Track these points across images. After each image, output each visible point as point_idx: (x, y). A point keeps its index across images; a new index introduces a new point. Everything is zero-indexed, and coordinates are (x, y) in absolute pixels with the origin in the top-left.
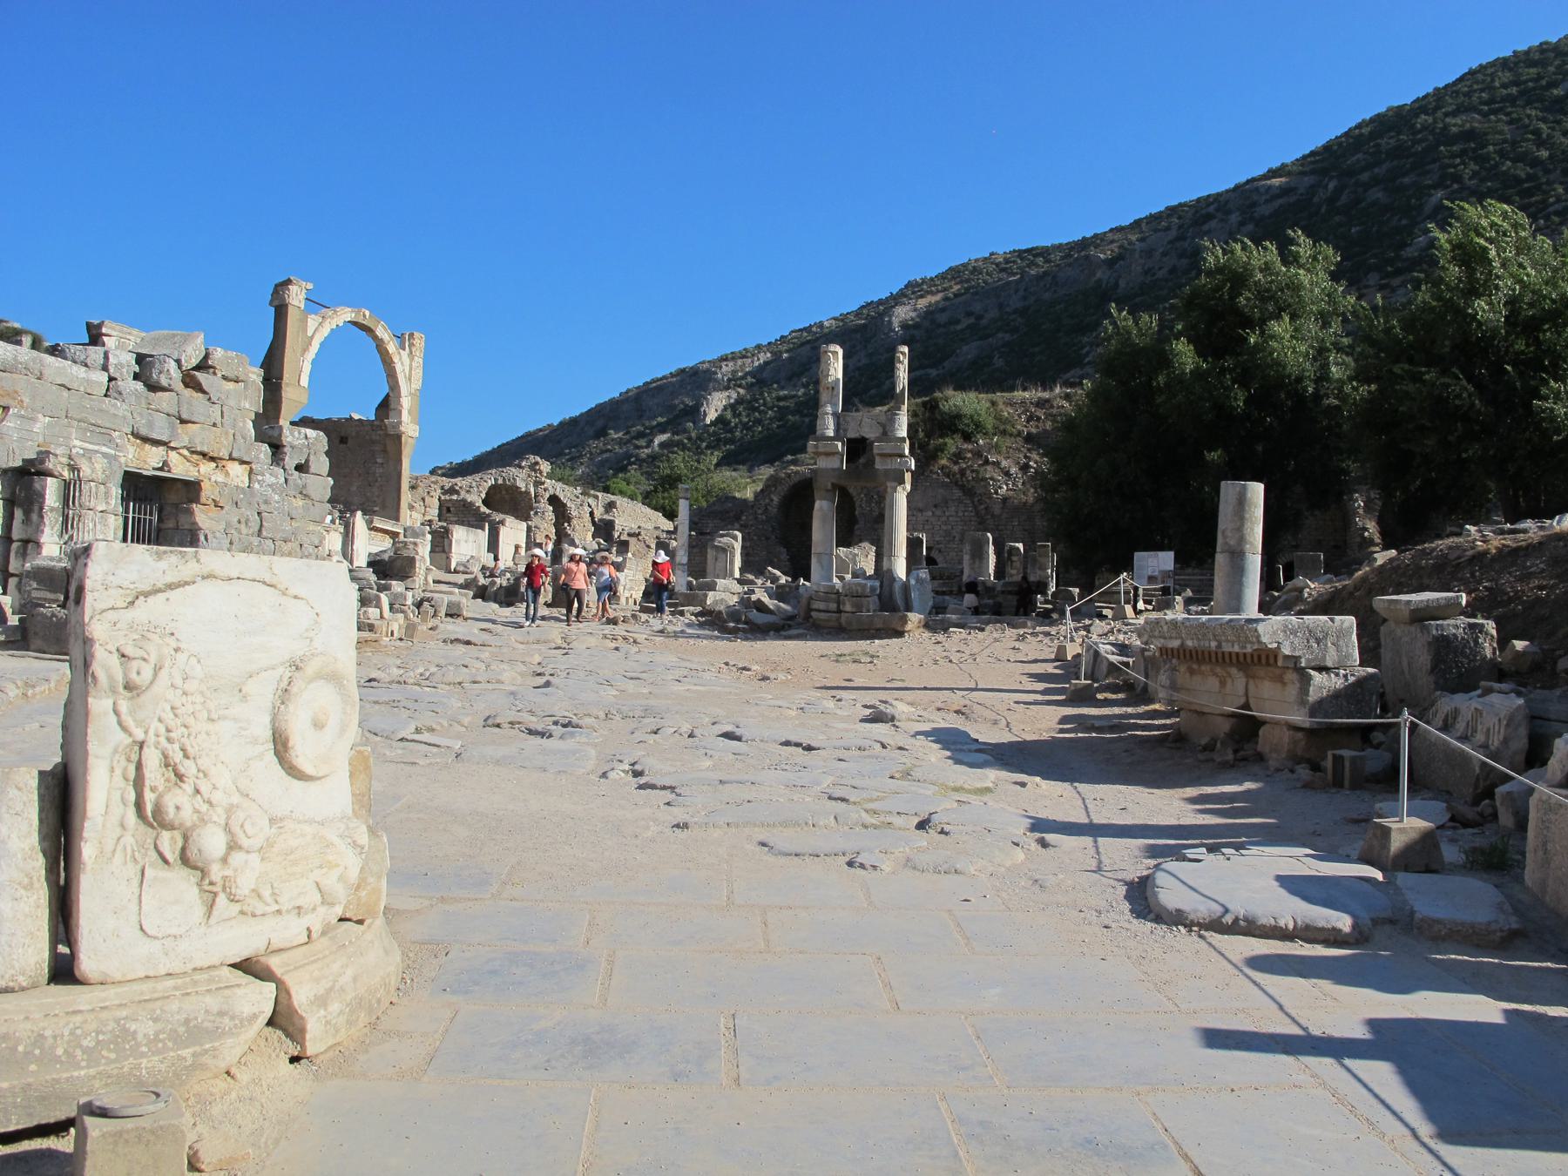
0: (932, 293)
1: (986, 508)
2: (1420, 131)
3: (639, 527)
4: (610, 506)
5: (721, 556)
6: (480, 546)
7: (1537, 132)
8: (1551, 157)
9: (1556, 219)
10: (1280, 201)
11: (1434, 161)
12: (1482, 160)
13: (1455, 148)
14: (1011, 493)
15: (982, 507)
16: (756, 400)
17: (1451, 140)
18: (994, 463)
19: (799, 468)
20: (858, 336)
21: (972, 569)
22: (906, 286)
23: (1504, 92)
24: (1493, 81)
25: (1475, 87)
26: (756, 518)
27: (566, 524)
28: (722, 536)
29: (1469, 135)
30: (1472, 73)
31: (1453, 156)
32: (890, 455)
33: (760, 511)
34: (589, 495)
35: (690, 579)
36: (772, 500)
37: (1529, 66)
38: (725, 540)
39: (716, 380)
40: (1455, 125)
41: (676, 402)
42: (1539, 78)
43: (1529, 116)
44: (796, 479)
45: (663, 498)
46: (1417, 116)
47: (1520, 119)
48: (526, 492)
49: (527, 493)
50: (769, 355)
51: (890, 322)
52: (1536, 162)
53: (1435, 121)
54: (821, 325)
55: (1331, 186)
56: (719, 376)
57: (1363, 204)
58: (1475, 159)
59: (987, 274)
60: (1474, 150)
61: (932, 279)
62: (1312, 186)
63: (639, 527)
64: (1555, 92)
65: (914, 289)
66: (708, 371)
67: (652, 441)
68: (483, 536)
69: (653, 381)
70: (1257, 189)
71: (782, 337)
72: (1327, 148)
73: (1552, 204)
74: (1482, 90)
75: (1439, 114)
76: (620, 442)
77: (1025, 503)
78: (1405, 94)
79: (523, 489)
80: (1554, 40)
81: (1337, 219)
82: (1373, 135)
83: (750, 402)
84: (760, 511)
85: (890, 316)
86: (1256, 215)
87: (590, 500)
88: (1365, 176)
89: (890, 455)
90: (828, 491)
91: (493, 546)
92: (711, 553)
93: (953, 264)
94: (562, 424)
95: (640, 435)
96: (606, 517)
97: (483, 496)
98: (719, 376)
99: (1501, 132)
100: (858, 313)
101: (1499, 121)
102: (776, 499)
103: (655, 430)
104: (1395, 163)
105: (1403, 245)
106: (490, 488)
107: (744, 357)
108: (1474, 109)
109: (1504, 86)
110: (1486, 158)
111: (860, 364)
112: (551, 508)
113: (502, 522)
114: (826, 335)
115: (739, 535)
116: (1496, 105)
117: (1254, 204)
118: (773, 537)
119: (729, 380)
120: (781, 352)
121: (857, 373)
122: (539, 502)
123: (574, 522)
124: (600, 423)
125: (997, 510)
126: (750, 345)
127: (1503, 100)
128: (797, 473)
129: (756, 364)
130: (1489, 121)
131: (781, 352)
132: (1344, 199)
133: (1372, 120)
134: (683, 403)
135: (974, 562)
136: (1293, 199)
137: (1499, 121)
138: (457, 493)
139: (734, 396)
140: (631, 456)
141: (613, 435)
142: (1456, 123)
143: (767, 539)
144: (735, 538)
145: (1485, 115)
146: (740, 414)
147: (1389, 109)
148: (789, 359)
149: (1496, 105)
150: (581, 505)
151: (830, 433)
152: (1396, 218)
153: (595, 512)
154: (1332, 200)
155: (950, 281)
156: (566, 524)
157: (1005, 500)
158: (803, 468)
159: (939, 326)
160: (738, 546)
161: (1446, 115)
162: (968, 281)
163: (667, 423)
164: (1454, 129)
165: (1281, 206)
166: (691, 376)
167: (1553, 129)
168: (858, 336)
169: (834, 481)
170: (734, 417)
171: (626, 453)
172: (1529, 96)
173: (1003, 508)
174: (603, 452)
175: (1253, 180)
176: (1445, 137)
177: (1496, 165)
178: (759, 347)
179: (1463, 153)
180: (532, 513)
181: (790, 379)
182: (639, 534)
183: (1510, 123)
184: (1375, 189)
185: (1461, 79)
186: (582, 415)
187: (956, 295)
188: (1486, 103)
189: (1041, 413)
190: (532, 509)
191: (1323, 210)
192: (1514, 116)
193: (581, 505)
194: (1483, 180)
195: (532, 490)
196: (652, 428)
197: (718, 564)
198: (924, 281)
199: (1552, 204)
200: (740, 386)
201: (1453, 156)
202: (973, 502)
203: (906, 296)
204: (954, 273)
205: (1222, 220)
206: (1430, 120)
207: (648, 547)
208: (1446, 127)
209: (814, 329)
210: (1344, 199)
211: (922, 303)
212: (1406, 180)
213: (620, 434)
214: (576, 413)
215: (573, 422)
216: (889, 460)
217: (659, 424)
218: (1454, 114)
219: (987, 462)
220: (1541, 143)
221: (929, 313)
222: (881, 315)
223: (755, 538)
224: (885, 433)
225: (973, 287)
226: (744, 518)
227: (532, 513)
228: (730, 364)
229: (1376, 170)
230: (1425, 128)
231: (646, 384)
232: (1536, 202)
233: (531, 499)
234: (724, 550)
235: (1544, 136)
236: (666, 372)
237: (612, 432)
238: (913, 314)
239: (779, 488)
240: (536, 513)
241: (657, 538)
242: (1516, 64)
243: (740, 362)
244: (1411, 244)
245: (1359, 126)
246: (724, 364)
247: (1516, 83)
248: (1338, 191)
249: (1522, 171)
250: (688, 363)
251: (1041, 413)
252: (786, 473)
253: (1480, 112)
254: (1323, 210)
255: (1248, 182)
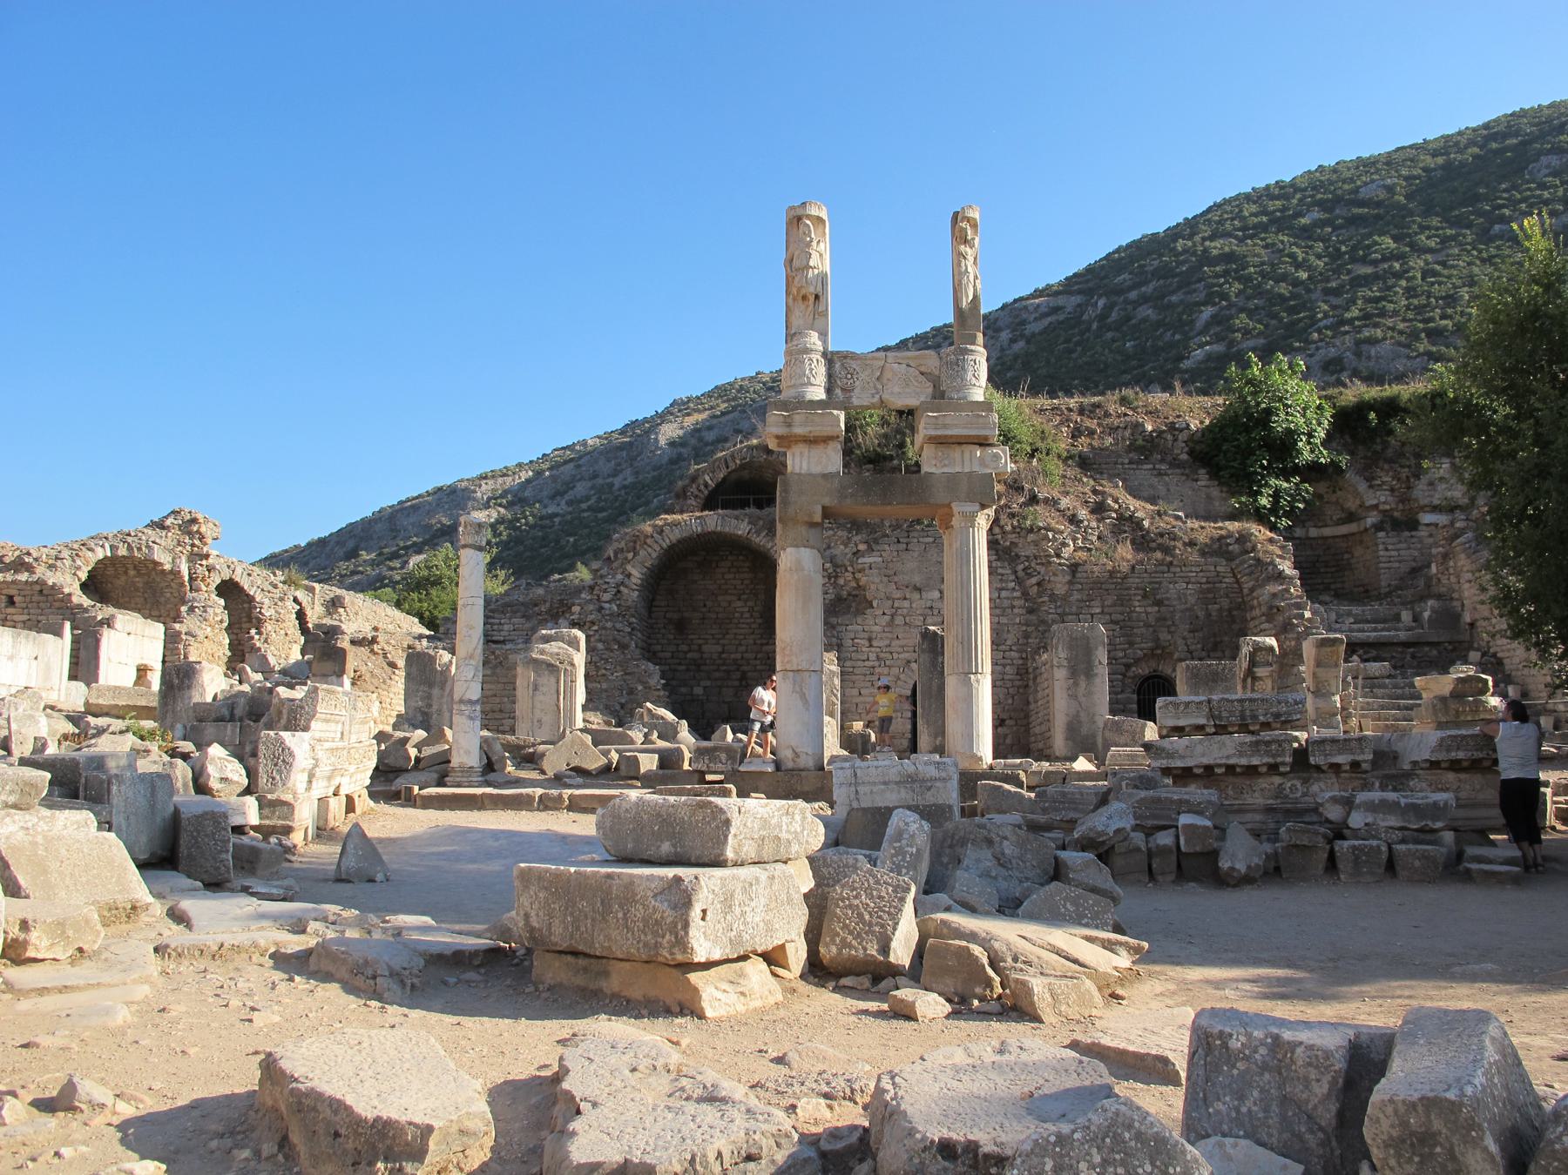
0: (699, 411)
1: (1039, 584)
2: (1181, 254)
3: (376, 629)
4: (334, 604)
5: (547, 681)
6: (48, 669)
7: (1292, 256)
8: (1310, 278)
9: (1329, 333)
10: (1049, 319)
11: (1199, 281)
12: (1245, 280)
13: (1218, 269)
14: (1082, 555)
15: (1034, 580)
16: (518, 520)
17: (1213, 262)
18: (1046, 501)
19: (677, 517)
20: (624, 454)
21: (1073, 697)
22: (671, 405)
23: (1256, 220)
24: (1241, 211)
25: (1226, 216)
26: (601, 609)
27: (253, 631)
28: (547, 639)
29: (1229, 257)
30: (1217, 206)
31: (1217, 276)
32: (961, 442)
33: (606, 597)
34: (297, 586)
35: (485, 733)
36: (629, 576)
37: (1272, 199)
38: (554, 647)
39: (475, 499)
40: (1215, 248)
41: (433, 521)
42: (1284, 209)
43: (1282, 242)
44: (675, 535)
45: (420, 601)
46: (1175, 241)
47: (1274, 245)
48: (171, 572)
49: (176, 573)
50: (531, 473)
51: (656, 440)
52: (1296, 283)
53: (1194, 245)
54: (584, 443)
55: (1101, 303)
56: (479, 494)
57: (1134, 321)
58: (1239, 279)
59: (754, 392)
60: (1236, 271)
61: (698, 398)
62: (1079, 305)
63: (376, 629)
64: (1303, 221)
65: (681, 407)
66: (466, 489)
67: (406, 562)
68: (58, 649)
69: (408, 500)
70: (1026, 308)
71: (544, 455)
72: (1090, 270)
73: (1321, 320)
74: (1233, 219)
75: (1197, 238)
76: (373, 563)
77: (1112, 573)
78: (1159, 223)
79: (167, 567)
80: (1288, 179)
81: (1109, 335)
82: (1132, 259)
83: (510, 522)
84: (606, 597)
85: (657, 434)
86: (1026, 332)
87: (300, 594)
88: (1133, 295)
89: (961, 442)
90: (812, 525)
91: (83, 665)
92: (524, 678)
93: (719, 383)
94: (309, 545)
95: (394, 556)
96: (328, 621)
97: (84, 576)
98: (479, 494)
99: (1258, 255)
100: (623, 432)
101: (1255, 245)
102: (637, 574)
103: (410, 551)
104: (1161, 282)
105: (1181, 358)
106: (99, 562)
107: (504, 475)
108: (1228, 235)
109: (1252, 215)
110: (1249, 279)
111: (626, 483)
112: (222, 602)
113: (108, 622)
114: (589, 453)
115: (581, 636)
116: (1250, 231)
117: (1023, 323)
118: (633, 644)
119: (489, 499)
120: (543, 471)
121: (623, 492)
122: (198, 590)
123: (268, 627)
124: (351, 544)
125: (1060, 585)
126: (511, 463)
127: (1255, 227)
128: (676, 524)
129: (517, 481)
130: (1247, 245)
131: (543, 471)
132: (1114, 316)
133: (1129, 246)
134: (440, 522)
135: (1076, 684)
136: (1061, 317)
137: (1255, 245)
138: (29, 569)
139: (495, 515)
140: (385, 578)
141: (364, 555)
142: (1216, 248)
143: (623, 647)
144: (574, 643)
145: (1241, 240)
146: (500, 534)
147: (1143, 237)
148: (550, 476)
149: (1250, 231)
150: (281, 599)
151: (817, 393)
152: (1169, 334)
153: (309, 612)
154: (1102, 317)
155: (717, 399)
156: (253, 631)
157: (1074, 567)
158: (685, 516)
159: (707, 444)
160: (580, 659)
161: (1204, 239)
162: (735, 399)
163: (424, 543)
164: (1215, 252)
165: (1051, 323)
166: (448, 495)
167: (1307, 253)
168: (624, 453)
169: (827, 501)
170: (494, 536)
171: (380, 574)
172: (1281, 222)
173: (1070, 583)
174: (354, 573)
175: (1021, 299)
176: (1206, 258)
177: (1259, 285)
178: (520, 465)
179: (1226, 273)
180: (184, 609)
181: (553, 497)
182: (374, 640)
183: (1266, 247)
184: (1145, 306)
185: (1209, 210)
186: (331, 535)
187: (723, 414)
188: (1239, 230)
189: (1091, 424)
190: (184, 602)
191: (1095, 326)
192: (1269, 241)
193: (281, 599)
194: (1248, 298)
195: (184, 569)
196: (406, 548)
197: (539, 697)
198: (689, 400)
199: (1321, 320)
200: (500, 505)
201: (1217, 276)
202: (1015, 572)
203: (672, 414)
204: (721, 392)
205: (992, 338)
206: (1190, 243)
207: (393, 665)
208: (1205, 251)
209: (578, 448)
210: (1114, 316)
211: (689, 421)
212: (1174, 298)
213: (373, 556)
214: (325, 533)
215: (322, 542)
216: (956, 452)
217: (415, 544)
218: (1212, 238)
219: (1033, 500)
220: (1298, 266)
221: (696, 431)
222: (647, 433)
223: (600, 646)
224: (939, 394)
225: (740, 405)
226: (576, 609)
227: (184, 609)
228: (490, 482)
229: (1143, 289)
230: (1185, 251)
231: (401, 503)
232: (1304, 318)
233: (182, 584)
234: (552, 669)
235: (1300, 259)
236: (422, 491)
237: (363, 552)
238: (681, 432)
239: (642, 553)
240: (192, 609)
241: (409, 647)
242: (1259, 198)
243: (500, 480)
244: (1188, 358)
245: (1117, 251)
246: (483, 482)
247: (1265, 213)
248: (1109, 308)
249: (1283, 289)
250: (446, 480)
251: (1091, 424)
252: (655, 526)
253: (1236, 237)
254: (1095, 326)
255: (1016, 301)
